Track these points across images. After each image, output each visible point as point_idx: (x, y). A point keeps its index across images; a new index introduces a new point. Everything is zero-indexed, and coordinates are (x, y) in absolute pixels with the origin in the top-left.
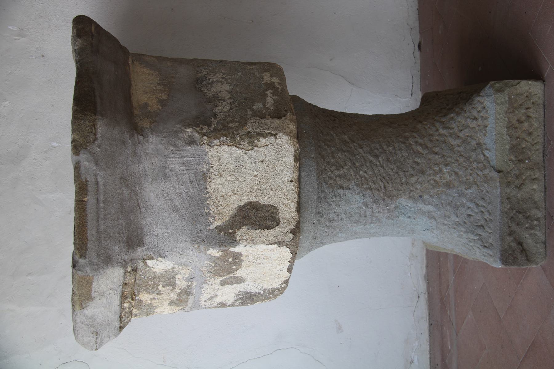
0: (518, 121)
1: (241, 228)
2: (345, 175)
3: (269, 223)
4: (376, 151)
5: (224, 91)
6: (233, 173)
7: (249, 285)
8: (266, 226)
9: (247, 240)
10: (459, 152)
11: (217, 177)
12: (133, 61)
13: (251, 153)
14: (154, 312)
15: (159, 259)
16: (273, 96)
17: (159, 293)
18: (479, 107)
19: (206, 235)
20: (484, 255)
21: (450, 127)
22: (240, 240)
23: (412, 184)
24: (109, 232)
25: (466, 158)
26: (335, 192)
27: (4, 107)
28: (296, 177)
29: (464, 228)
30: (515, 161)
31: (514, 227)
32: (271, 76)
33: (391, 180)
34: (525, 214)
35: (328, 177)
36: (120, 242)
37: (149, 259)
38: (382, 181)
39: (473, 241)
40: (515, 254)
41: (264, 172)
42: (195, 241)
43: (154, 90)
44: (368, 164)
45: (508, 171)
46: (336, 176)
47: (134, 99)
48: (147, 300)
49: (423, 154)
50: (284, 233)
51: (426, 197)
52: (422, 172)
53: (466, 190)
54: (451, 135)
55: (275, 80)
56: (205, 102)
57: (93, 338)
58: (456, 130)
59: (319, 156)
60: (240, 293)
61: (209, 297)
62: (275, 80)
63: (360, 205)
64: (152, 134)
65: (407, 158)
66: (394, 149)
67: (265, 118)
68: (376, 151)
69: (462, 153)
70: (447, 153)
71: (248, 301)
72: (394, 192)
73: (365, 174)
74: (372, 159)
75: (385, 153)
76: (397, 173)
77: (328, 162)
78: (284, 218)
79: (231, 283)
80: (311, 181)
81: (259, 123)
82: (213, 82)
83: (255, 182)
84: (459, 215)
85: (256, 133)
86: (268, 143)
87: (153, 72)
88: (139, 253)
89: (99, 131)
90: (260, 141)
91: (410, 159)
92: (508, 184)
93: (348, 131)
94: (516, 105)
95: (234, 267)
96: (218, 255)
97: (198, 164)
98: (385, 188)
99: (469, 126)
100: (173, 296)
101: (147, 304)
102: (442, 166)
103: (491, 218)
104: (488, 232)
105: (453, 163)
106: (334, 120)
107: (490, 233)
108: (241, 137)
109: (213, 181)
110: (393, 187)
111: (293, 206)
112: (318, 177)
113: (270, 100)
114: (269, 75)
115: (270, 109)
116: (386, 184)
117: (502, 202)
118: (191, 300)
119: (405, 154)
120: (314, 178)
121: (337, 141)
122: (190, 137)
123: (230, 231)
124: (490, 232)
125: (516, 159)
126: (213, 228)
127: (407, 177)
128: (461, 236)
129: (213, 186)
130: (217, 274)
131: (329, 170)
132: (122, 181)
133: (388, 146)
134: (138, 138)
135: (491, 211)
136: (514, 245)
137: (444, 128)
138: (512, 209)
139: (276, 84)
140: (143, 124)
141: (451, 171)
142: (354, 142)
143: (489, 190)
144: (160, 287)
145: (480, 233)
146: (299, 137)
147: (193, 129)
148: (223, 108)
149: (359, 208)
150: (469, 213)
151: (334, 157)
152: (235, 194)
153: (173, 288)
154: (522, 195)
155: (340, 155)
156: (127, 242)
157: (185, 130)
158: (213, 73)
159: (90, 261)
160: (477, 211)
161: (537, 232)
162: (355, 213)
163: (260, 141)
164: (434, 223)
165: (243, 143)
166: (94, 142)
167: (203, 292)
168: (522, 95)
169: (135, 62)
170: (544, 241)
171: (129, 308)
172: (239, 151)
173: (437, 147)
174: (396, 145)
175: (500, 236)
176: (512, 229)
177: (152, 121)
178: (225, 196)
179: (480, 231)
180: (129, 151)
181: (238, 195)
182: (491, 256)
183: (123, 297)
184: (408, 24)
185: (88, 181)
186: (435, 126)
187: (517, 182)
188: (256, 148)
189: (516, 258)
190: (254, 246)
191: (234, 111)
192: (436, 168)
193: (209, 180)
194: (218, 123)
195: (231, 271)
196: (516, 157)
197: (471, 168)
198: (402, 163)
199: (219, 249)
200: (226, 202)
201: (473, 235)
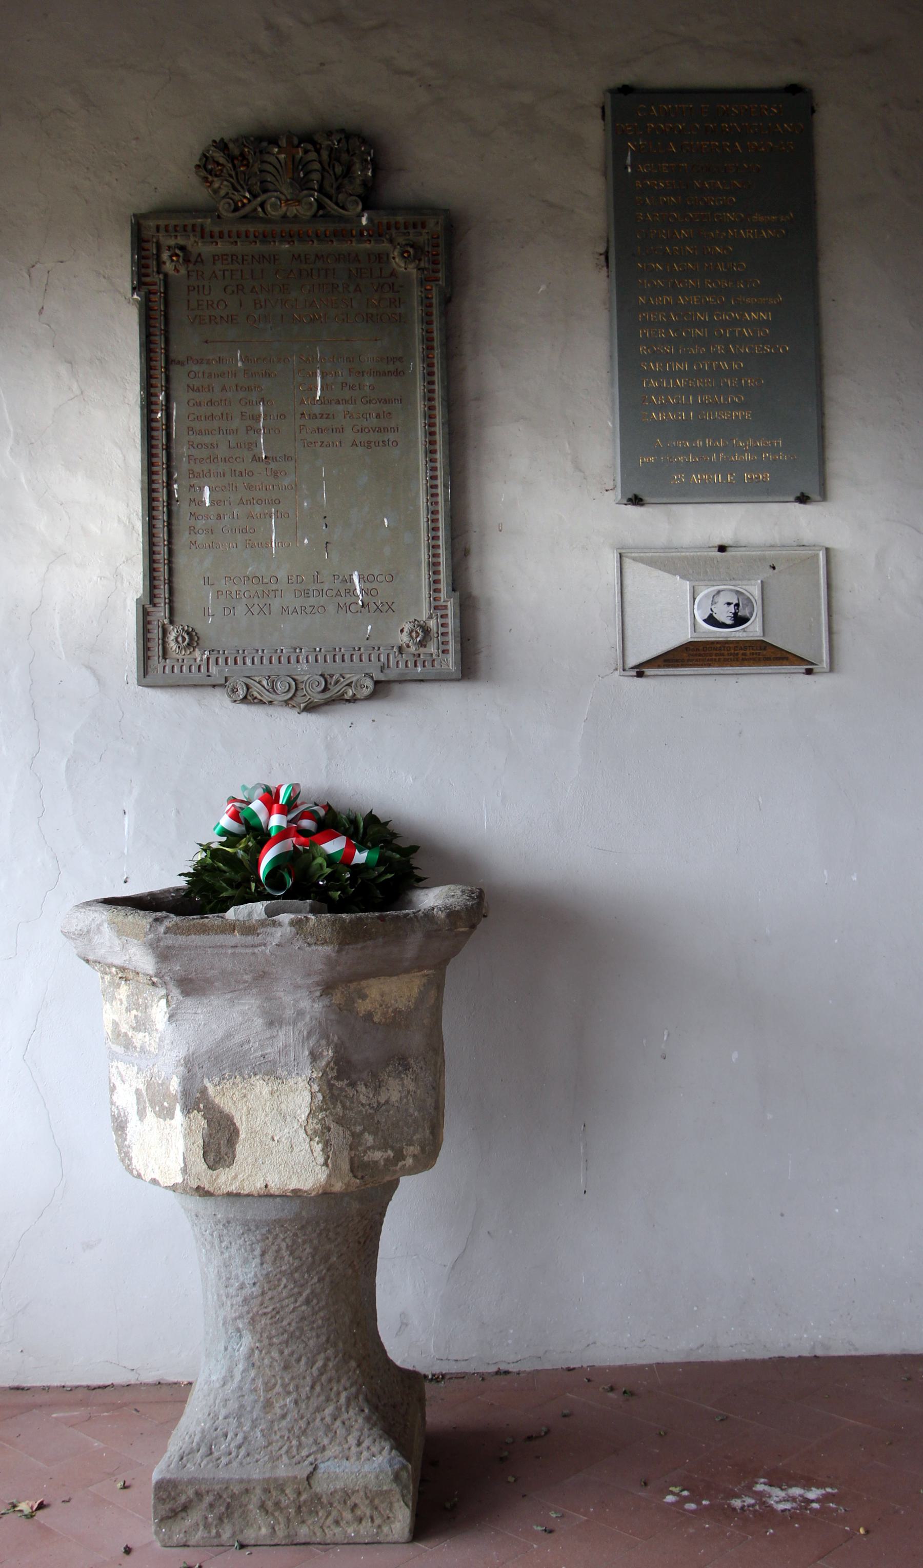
0: (355, 1505)
1: (205, 1119)
2: (281, 1258)
3: (211, 1156)
4: (315, 1301)
5: (389, 1095)
6: (275, 1109)
7: (136, 1126)
8: (207, 1151)
9: (190, 1127)
10: (314, 1420)
11: (270, 1089)
12: (427, 975)
13: (302, 1132)
14: (106, 1001)
15: (167, 1016)
16: (384, 1159)
17: (128, 1010)
18: (374, 1449)
19: (195, 1074)
20: (171, 1456)
21: (350, 1408)
22: (189, 1118)
23: (270, 1353)
24: (197, 960)
25: (305, 1430)
26: (258, 1244)
27: (406, 777)
28: (272, 1192)
29: (209, 1428)
30: (299, 1502)
31: (208, 1499)
32: (414, 1156)
33: (276, 1323)
34: (225, 1515)
35: (277, 1235)
36: (185, 971)
37: (168, 1002)
38: (273, 1309)
39: (191, 1440)
40: (170, 1501)
41: (278, 1149)
42: (189, 1061)
43: (387, 1005)
44: (296, 1290)
45: (285, 1491)
46: (279, 1245)
47: (372, 981)
48: (120, 995)
49: (311, 1368)
50: (198, 1175)
51: (253, 1373)
52: (286, 1367)
53: (262, 1431)
54: (338, 1409)
55: (409, 1161)
56: (371, 1071)
57: (76, 930)
58: (345, 1416)
59: (304, 1222)
60: (126, 1114)
61: (122, 1072)
62: (409, 1161)
63: (241, 1279)
64: (324, 1007)
65: (306, 1345)
66: (319, 1327)
67: (351, 1149)
68: (315, 1301)
69: (312, 1425)
70: (313, 1403)
71: (116, 1124)
72: (258, 1327)
73: (282, 1286)
74: (305, 1295)
75: (313, 1315)
76: (286, 1331)
77: (297, 1235)
78: (218, 1176)
79: (138, 1103)
80: (270, 1211)
81: (343, 1142)
82: (402, 1079)
83: (264, 1138)
84: (227, 1420)
85: (328, 1140)
86: (315, 1154)
87: (413, 1001)
88: (174, 991)
89: (320, 948)
90: (318, 1144)
91: (304, 1349)
92: (267, 1491)
93: (343, 1262)
94: (377, 1501)
95: (157, 1109)
96: (171, 1089)
97: (286, 1064)
98: (265, 1314)
99: (349, 1434)
100: (124, 1028)
101: (116, 994)
102: (294, 1395)
103: (220, 1466)
104: (202, 1461)
105: (299, 1411)
106: (359, 1243)
107: (200, 1465)
108: (323, 1119)
109: (265, 1083)
110: (266, 1325)
111: (233, 1188)
112: (275, 1221)
113: (378, 1155)
114: (416, 1152)
115: (365, 1155)
116: (270, 1316)
117: (241, 1481)
118: (119, 1050)
119: (311, 1343)
120: (274, 1215)
121: (328, 1247)
122: (321, 1053)
123: (201, 1106)
124: (202, 1465)
125: (302, 1503)
126: (205, 1083)
127: (279, 1346)
128: (198, 1423)
129: (258, 1083)
130: (149, 1085)
131: (286, 1235)
132: (261, 973)
133: (322, 1318)
134: (317, 990)
135: (230, 1466)
136: (183, 1499)
137: (348, 1400)
138: (233, 1496)
139: (403, 1163)
140: (336, 995)
141: (288, 1410)
142: (328, 1270)
143: (259, 1462)
144: (134, 1012)
145: (200, 1451)
146: (325, 1195)
147: (333, 1057)
148: (363, 1093)
149: (237, 1277)
150: (229, 1436)
151: (304, 1242)
152: (249, 1111)
153: (134, 1029)
154: (252, 1511)
155: (308, 1250)
156: (186, 979)
157: (330, 1048)
158: (416, 1078)
159: (162, 938)
160: (232, 1445)
161: (200, 1533)
162: (230, 1273)
163: (318, 1144)
164: (217, 1385)
165: (315, 1121)
166: (305, 942)
167: (128, 1065)
168: (391, 1510)
169: (426, 978)
170: (189, 1543)
171: (110, 973)
172: (304, 1117)
173: (322, 1389)
174: (324, 1330)
175: (195, 1479)
176: (204, 1497)
177: (342, 1006)
178: (245, 1099)
179: (203, 1450)
180: (299, 981)
181: (247, 1115)
182: (169, 1466)
183: (123, 969)
184: (546, 1351)
185: (258, 936)
186: (351, 1386)
187: (269, 1504)
188: (308, 1140)
189: (165, 1502)
190: (182, 1136)
191: (359, 1109)
192: (291, 1388)
193: (266, 1078)
194: (341, 1089)
195: (153, 1104)
196: (305, 1502)
197: (291, 1438)
198: (298, 1338)
199: (179, 1091)
200: (239, 1100)
201: (198, 1440)
